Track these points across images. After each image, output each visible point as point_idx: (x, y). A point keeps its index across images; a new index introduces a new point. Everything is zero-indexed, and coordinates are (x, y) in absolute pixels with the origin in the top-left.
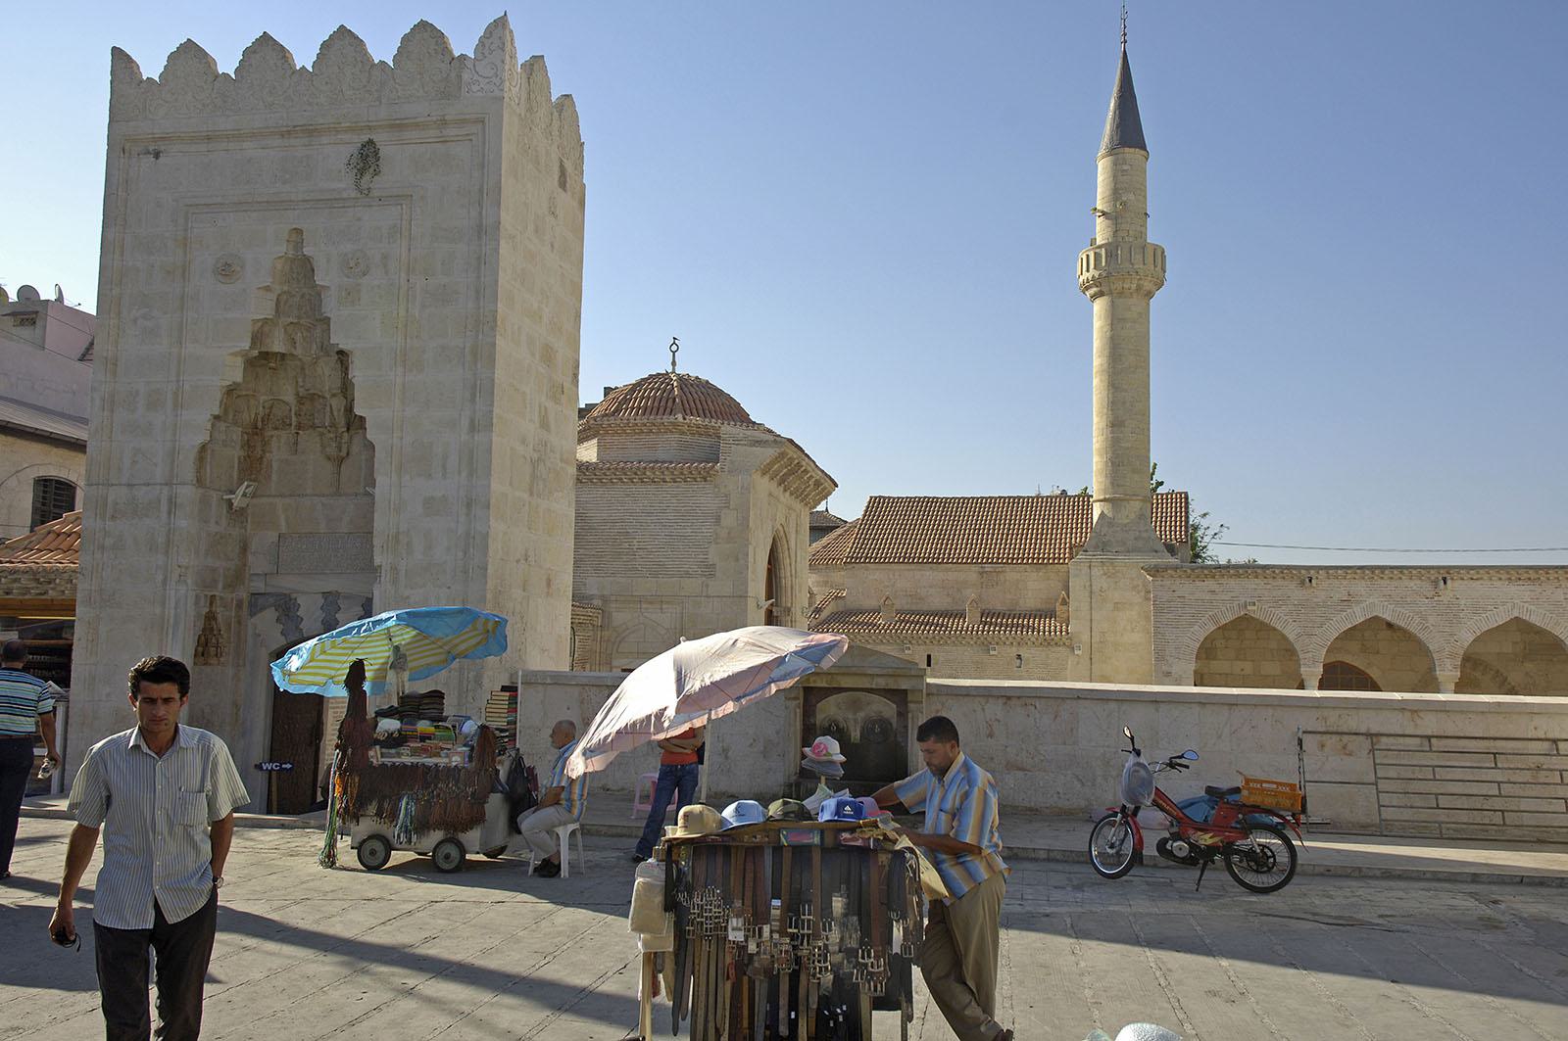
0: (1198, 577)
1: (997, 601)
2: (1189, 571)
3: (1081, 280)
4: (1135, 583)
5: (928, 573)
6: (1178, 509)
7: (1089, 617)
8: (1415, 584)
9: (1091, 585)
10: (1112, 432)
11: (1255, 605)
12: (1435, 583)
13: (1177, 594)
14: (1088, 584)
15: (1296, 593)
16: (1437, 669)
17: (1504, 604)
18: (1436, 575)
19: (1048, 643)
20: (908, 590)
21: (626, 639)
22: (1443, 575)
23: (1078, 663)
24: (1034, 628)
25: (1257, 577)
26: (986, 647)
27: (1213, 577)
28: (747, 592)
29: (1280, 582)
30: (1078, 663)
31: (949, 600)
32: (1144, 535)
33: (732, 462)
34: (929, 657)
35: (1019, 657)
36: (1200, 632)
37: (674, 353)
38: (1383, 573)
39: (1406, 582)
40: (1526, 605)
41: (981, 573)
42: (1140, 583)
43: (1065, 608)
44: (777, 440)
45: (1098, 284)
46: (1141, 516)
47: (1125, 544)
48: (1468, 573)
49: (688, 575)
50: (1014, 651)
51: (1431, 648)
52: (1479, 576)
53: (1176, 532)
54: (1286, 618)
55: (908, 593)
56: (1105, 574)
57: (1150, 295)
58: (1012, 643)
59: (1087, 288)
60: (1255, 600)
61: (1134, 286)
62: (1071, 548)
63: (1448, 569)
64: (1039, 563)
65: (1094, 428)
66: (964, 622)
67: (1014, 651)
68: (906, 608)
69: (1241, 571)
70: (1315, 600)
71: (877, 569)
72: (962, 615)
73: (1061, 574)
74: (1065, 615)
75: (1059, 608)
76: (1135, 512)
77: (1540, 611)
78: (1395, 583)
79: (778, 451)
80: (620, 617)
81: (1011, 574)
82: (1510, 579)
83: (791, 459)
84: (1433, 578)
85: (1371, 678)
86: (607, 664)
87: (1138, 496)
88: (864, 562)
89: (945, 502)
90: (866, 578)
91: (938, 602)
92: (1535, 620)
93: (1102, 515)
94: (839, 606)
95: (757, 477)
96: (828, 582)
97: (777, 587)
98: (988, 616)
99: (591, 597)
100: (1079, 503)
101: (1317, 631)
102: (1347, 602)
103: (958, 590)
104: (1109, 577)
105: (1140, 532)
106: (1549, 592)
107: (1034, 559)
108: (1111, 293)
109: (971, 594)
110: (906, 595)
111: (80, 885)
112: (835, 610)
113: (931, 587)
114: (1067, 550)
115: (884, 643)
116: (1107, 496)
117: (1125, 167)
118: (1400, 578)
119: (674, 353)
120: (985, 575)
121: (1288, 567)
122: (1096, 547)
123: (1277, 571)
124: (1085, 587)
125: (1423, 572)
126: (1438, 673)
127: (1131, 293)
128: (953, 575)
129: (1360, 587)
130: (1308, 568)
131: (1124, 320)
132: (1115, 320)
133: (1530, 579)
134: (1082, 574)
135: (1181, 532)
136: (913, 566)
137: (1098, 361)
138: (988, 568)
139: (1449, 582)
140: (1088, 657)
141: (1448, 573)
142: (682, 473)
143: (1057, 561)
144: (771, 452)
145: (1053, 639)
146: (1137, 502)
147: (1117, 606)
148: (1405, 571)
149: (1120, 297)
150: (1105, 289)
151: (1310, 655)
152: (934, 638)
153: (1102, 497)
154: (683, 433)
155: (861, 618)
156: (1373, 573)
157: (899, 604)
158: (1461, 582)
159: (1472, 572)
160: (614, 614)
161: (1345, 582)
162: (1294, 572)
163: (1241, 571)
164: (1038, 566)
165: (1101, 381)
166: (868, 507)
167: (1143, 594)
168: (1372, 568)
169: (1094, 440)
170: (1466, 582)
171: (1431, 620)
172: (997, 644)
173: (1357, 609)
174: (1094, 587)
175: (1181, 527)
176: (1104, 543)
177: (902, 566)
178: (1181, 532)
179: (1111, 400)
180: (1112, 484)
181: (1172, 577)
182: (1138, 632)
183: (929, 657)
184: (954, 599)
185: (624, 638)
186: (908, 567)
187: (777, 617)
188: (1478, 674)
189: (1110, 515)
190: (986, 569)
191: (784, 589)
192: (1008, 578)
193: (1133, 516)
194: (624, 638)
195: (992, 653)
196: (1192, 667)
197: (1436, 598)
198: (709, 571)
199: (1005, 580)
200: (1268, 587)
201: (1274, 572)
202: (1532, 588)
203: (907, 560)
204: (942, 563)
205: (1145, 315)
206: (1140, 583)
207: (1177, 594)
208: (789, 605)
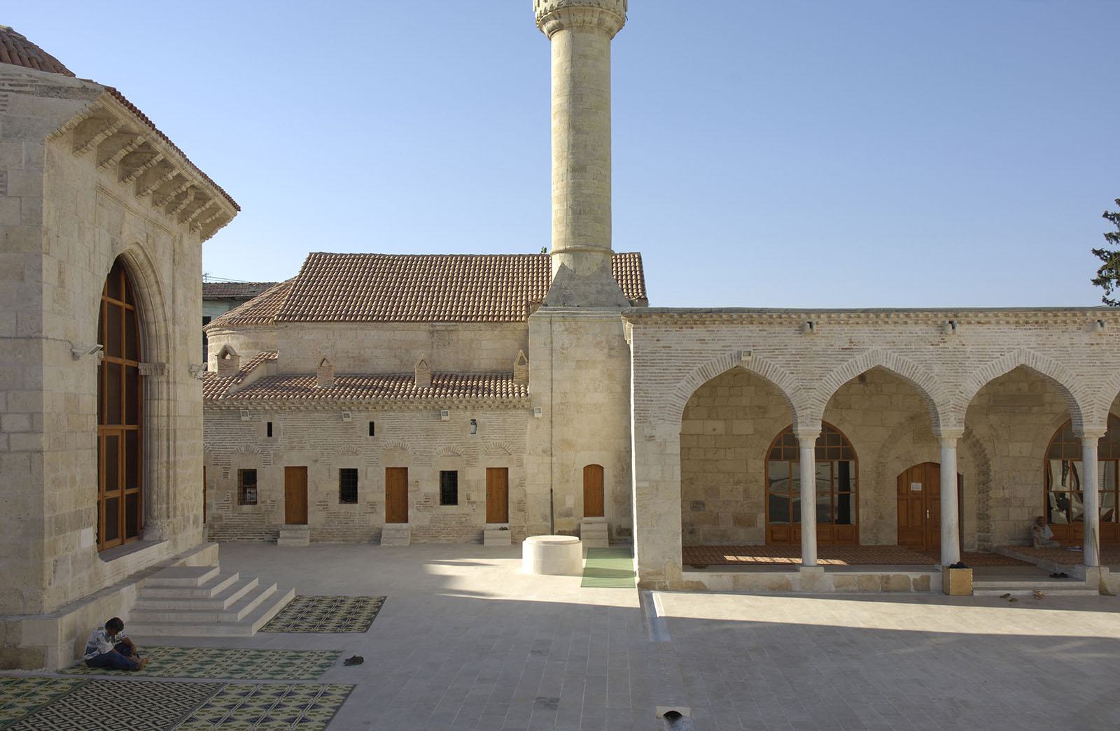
0: (685, 324)
1: (449, 361)
2: (676, 316)
3: (538, 12)
4: (599, 339)
5: (372, 333)
6: (632, 264)
7: (549, 377)
8: (919, 329)
9: (552, 342)
10: (573, 178)
11: (750, 355)
12: (941, 328)
13: (662, 343)
14: (549, 340)
15: (796, 342)
16: (941, 425)
17: (1010, 350)
18: (944, 319)
19: (505, 406)
20: (350, 351)
22: (949, 319)
23: (538, 427)
24: (490, 390)
25: (751, 323)
26: (438, 412)
27: (703, 323)
29: (777, 329)
30: (538, 427)
31: (397, 362)
32: (607, 288)
34: (372, 425)
35: (474, 422)
36: (688, 386)
38: (888, 316)
39: (912, 327)
40: (1032, 351)
41: (432, 333)
42: (603, 339)
43: (523, 367)
44: (88, 88)
45: (557, 16)
46: (603, 269)
47: (586, 297)
48: (976, 316)
50: (468, 416)
51: (935, 401)
52: (986, 319)
53: (632, 290)
54: (782, 369)
55: (351, 355)
56: (567, 330)
57: (610, 34)
58: (466, 407)
59: (545, 21)
60: (751, 349)
61: (595, 20)
62: (527, 306)
63: (955, 312)
64: (493, 321)
65: (553, 175)
66: (413, 384)
67: (468, 416)
69: (735, 316)
70: (814, 348)
71: (314, 328)
72: (411, 378)
73: (517, 332)
74: (524, 375)
75: (517, 369)
76: (597, 265)
77: (1046, 357)
78: (901, 328)
79: (90, 105)
81: (465, 333)
82: (1017, 322)
83: (124, 132)
84: (939, 322)
85: (843, 434)
87: (600, 246)
88: (299, 321)
89: (393, 260)
90: (302, 338)
91: (384, 363)
92: (1041, 367)
93: (563, 267)
94: (272, 370)
95: (62, 151)
96: (258, 344)
97: (145, 341)
98: (440, 379)
100: (533, 261)
101: (816, 384)
102: (849, 350)
103: (407, 350)
104: (571, 332)
105: (602, 285)
106: (1055, 338)
107: (488, 317)
108: (570, 26)
109: (421, 354)
110: (348, 357)
111: (92, 528)
112: (265, 374)
113: (376, 348)
114: (524, 308)
115: (318, 411)
116: (568, 247)
118: (906, 323)
120: (436, 335)
121: (787, 311)
122: (557, 301)
123: (775, 315)
124: (545, 344)
125: (930, 315)
126: (941, 429)
127: (592, 28)
128: (400, 334)
129: (862, 333)
130: (808, 312)
131: (585, 56)
132: (577, 57)
133: (1037, 323)
134: (545, 332)
135: (637, 290)
136: (355, 325)
137: (557, 100)
138: (439, 326)
139: (958, 326)
140: (549, 420)
141: (956, 316)
143: (511, 319)
144: (76, 109)
145: (511, 402)
146: (600, 254)
147: (580, 364)
148: (912, 315)
149: (581, 31)
150: (564, 21)
151: (808, 411)
152: (378, 403)
153: (562, 248)
155: (294, 383)
156: (877, 316)
157: (342, 366)
158: (967, 326)
159: (980, 315)
161: (847, 328)
162: (793, 316)
163: (735, 316)
164: (493, 324)
165: (561, 122)
166: (307, 263)
167: (606, 350)
168: (877, 312)
169: (553, 187)
170: (972, 326)
171: (937, 369)
172: (450, 408)
173: (859, 358)
174: (554, 344)
175: (637, 285)
176: (566, 296)
177: (343, 325)
178: (637, 290)
179: (571, 143)
180: (573, 233)
181: (657, 323)
182: (601, 392)
183: (372, 425)
184: (401, 361)
186: (350, 325)
187: (146, 376)
189: (571, 267)
190: (437, 328)
191: (154, 338)
192: (460, 337)
193: (595, 268)
195: (444, 418)
196: (678, 429)
197: (942, 345)
199: (458, 340)
200: (765, 333)
201: (771, 317)
202: (1038, 332)
203: (350, 318)
204: (388, 321)
205: (605, 54)
206: (603, 339)
207: (662, 343)
208: (164, 361)
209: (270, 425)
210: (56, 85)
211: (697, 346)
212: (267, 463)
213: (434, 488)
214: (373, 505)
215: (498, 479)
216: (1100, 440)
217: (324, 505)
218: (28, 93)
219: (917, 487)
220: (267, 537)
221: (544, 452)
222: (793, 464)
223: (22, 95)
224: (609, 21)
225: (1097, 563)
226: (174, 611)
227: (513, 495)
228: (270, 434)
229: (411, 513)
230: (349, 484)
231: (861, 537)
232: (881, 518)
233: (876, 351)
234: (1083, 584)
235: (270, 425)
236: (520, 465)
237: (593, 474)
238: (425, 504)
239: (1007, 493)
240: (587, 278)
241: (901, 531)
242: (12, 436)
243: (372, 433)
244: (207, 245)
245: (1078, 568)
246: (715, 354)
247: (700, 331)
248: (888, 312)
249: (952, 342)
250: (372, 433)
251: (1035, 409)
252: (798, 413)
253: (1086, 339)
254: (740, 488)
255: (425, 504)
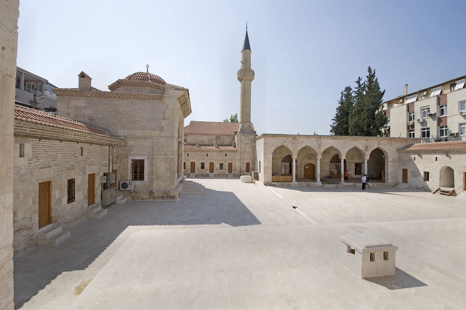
12: (318, 139)
21: (133, 150)
28: (174, 135)
32: (251, 129)
33: (169, 95)
34: (207, 154)
36: (274, 148)
37: (148, 68)
49: (154, 130)
68: (209, 144)
78: (311, 139)
80: (130, 143)
86: (126, 158)
99: (120, 136)
117: (248, 54)
119: (148, 68)
121: (291, 135)
129: (305, 139)
142: (152, 97)
154: (152, 87)
160: (128, 142)
161: (302, 138)
173: (304, 144)
183: (207, 154)
185: (132, 150)
188: (312, 157)
193: (248, 126)
194: (132, 150)
198: (162, 129)
205: (250, 85)
207: (269, 140)
209: (188, 154)
210: (178, 88)
211: (275, 141)
212: (187, 161)
213: (219, 166)
214: (207, 170)
215: (230, 165)
216: (368, 160)
217: (198, 169)
218: (172, 89)
219: (307, 167)
220: (188, 175)
221: (239, 160)
222: (286, 163)
223: (171, 90)
224: (251, 78)
225: (295, 181)
226: (193, 189)
227: (233, 168)
228: (188, 156)
229: (214, 171)
230: (221, 166)
231: (298, 176)
232: (301, 173)
233: (307, 143)
234: (341, 185)
235: (188, 154)
236: (235, 162)
237: (248, 164)
238: (217, 170)
239: (323, 169)
240: (247, 127)
241: (305, 175)
242: (169, 156)
243: (207, 156)
244: (185, 119)
245: (340, 182)
246: (279, 142)
247: (276, 138)
248: (309, 135)
249: (320, 142)
250: (207, 156)
251: (328, 154)
252: (293, 154)
253: (342, 141)
254: (277, 167)
255: (217, 170)
